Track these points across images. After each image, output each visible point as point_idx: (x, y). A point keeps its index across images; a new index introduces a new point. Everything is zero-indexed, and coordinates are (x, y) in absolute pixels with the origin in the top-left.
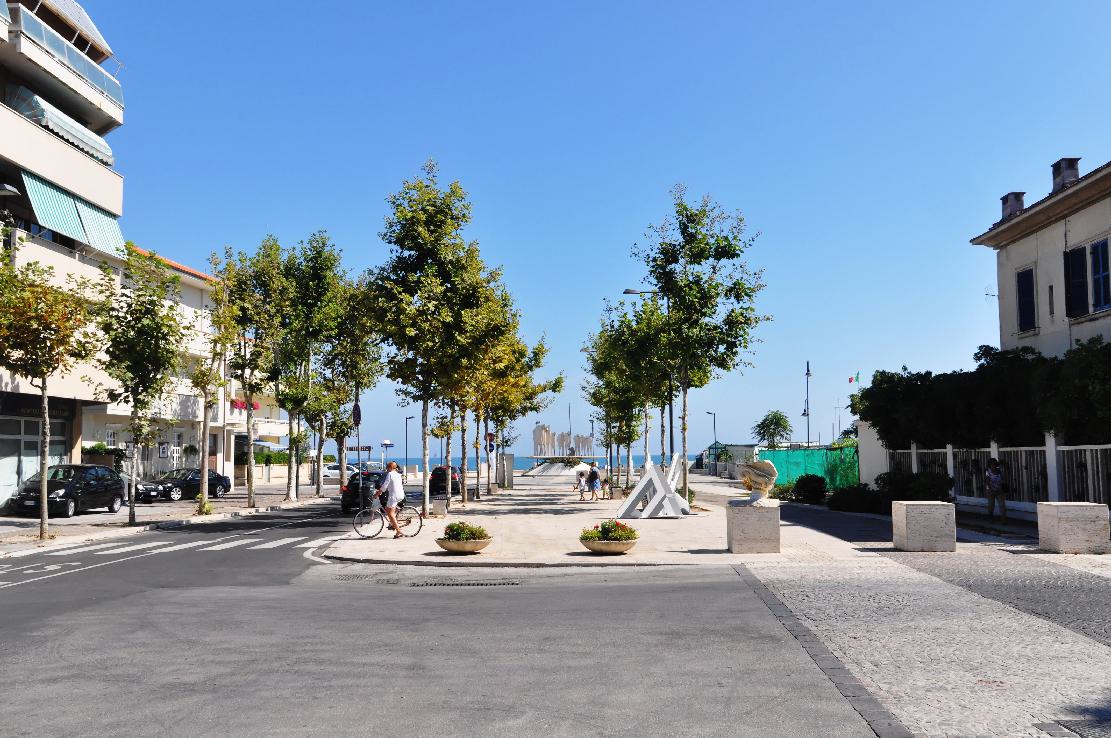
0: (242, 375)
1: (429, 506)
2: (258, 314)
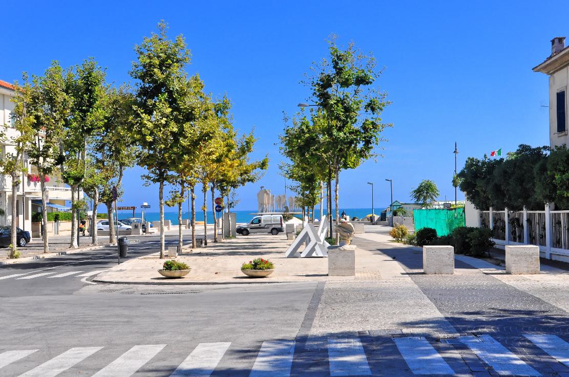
0: (37, 162)
1: (165, 252)
2: (48, 119)
